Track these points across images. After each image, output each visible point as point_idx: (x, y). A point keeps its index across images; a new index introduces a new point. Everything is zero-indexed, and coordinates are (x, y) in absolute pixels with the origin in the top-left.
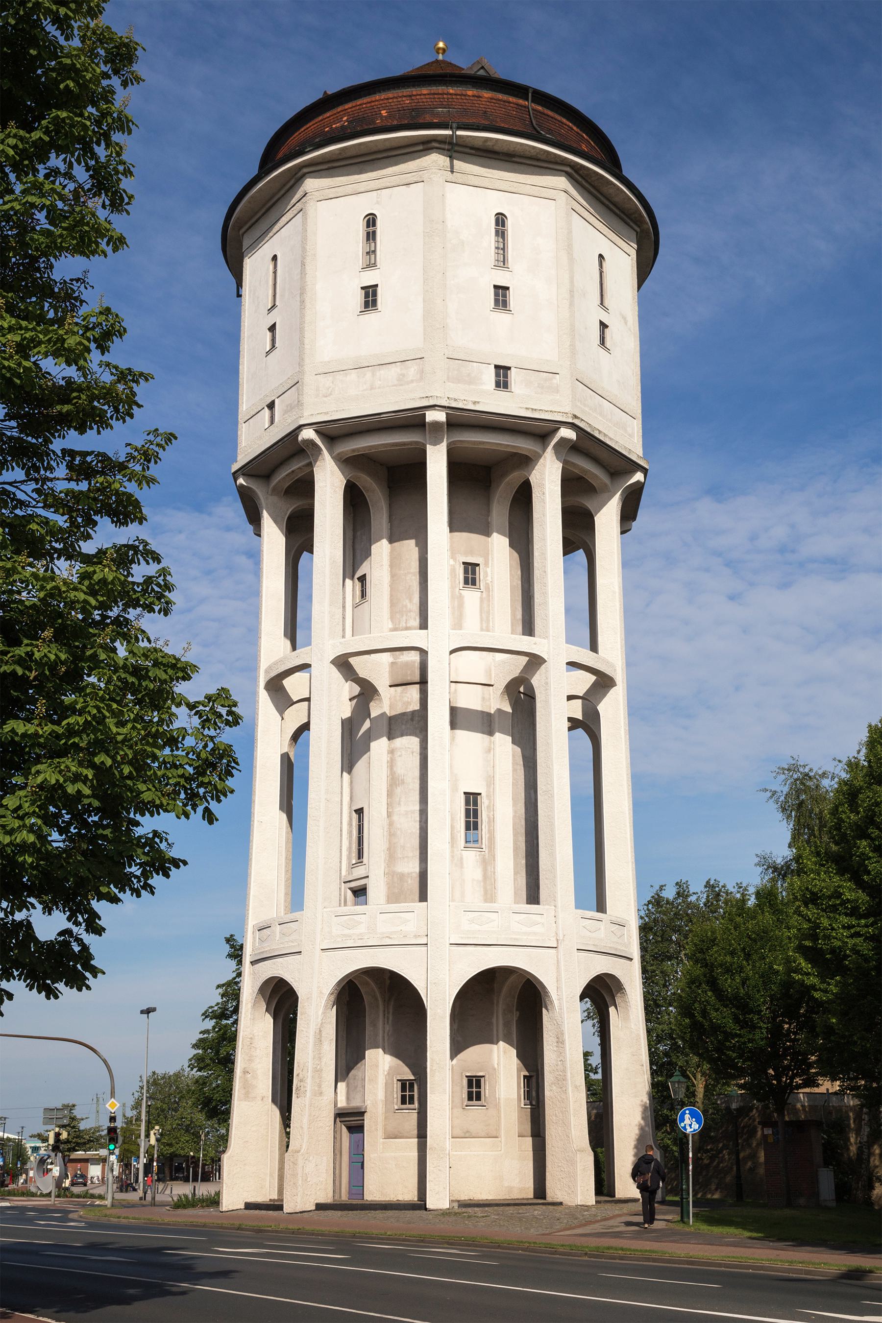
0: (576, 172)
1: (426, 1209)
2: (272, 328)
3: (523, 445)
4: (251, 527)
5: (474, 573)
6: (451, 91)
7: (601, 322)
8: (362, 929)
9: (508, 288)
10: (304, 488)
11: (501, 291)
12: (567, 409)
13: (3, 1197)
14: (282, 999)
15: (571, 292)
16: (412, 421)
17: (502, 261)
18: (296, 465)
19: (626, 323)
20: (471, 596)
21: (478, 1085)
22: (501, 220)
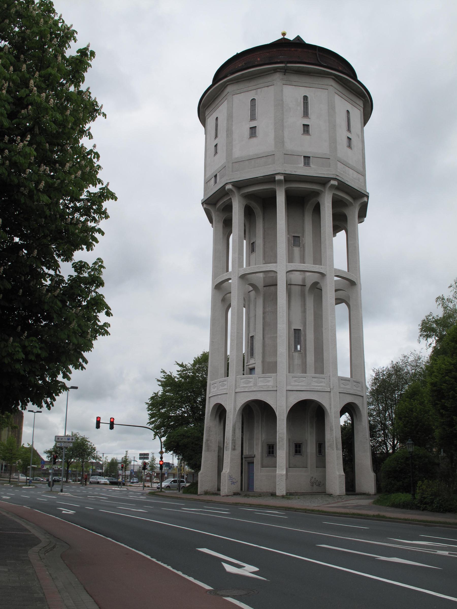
0: (336, 78)
1: (253, 491)
2: (216, 146)
4: (211, 225)
7: (348, 137)
8: (251, 384)
9: (309, 125)
10: (228, 208)
11: (306, 126)
12: (334, 173)
14: (220, 412)
16: (270, 179)
17: (306, 114)
19: (359, 137)
21: (269, 451)
22: (305, 98)
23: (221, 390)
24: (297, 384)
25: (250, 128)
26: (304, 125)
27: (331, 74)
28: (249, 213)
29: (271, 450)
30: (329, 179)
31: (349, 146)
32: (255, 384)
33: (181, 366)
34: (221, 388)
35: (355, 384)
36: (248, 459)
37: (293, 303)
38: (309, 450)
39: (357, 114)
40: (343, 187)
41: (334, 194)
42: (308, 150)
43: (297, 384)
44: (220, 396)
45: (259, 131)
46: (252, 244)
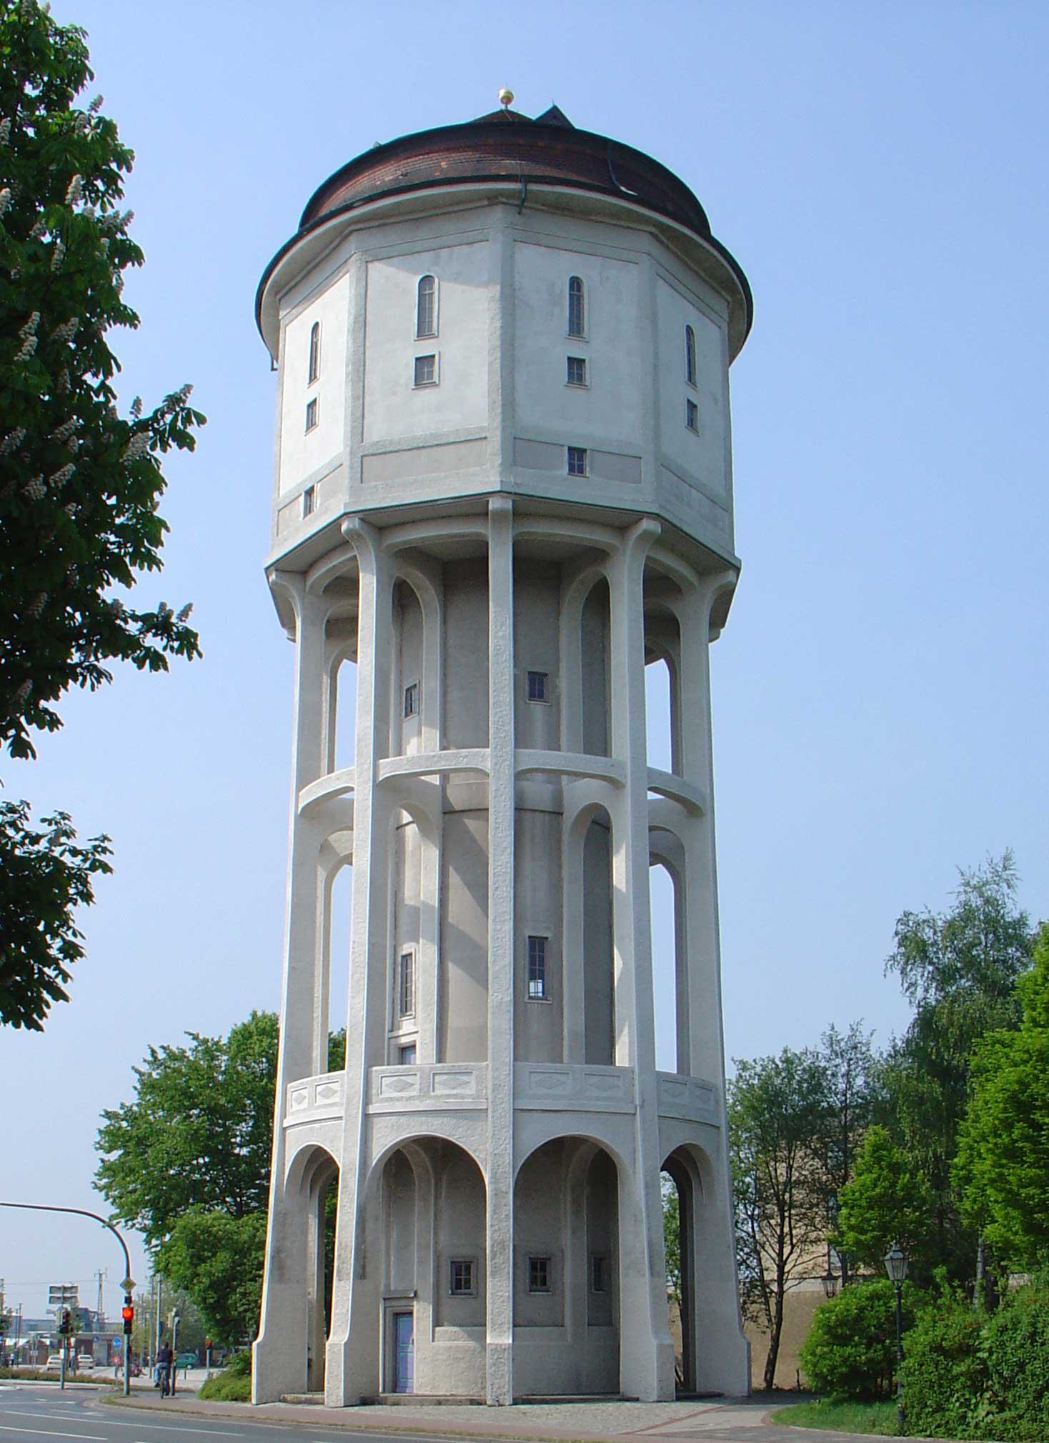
2: (312, 405)
3: (600, 537)
4: (285, 633)
5: (541, 683)
6: (521, 141)
9: (583, 361)
10: (346, 586)
11: (576, 365)
13: (8, 1386)
15: (656, 366)
16: (474, 508)
17: (576, 327)
18: (337, 560)
20: (538, 708)
21: (544, 1269)
22: (575, 284)
23: (320, 1107)
24: (545, 1091)
25: (417, 359)
26: (569, 358)
27: (648, 221)
28: (401, 601)
29: (463, 1278)
30: (640, 515)
31: (691, 423)
32: (424, 1093)
33: (195, 1038)
34: (321, 1101)
35: (698, 1092)
36: (394, 1303)
37: (528, 865)
38: (568, 1278)
39: (710, 337)
40: (673, 537)
41: (648, 558)
42: (582, 431)
43: (545, 1091)
44: (317, 1125)
45: (445, 371)
46: (408, 690)
